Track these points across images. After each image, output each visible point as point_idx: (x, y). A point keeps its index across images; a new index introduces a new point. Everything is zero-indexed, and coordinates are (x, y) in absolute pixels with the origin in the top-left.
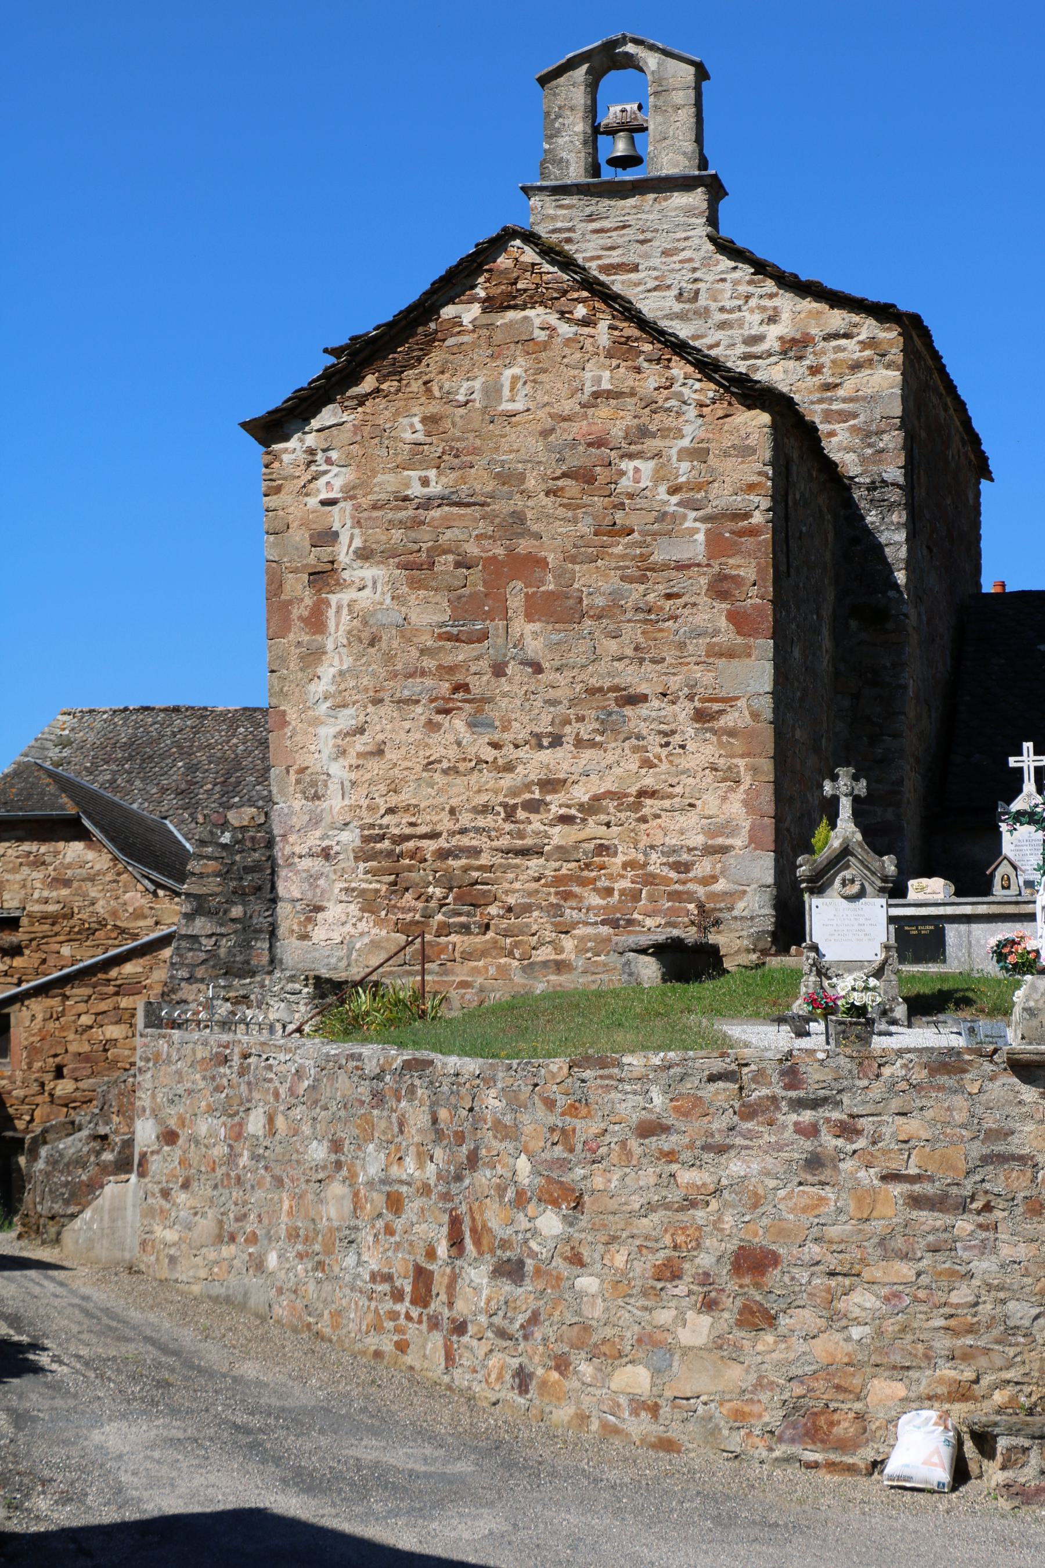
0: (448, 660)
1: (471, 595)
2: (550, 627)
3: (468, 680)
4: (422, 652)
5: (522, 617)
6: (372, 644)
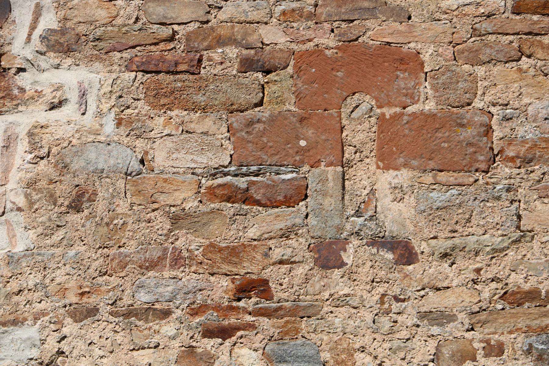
0: (225, 234)
1: (272, 119)
2: (428, 178)
3: (266, 274)
4: (176, 220)
5: (371, 162)
6: (76, 206)
